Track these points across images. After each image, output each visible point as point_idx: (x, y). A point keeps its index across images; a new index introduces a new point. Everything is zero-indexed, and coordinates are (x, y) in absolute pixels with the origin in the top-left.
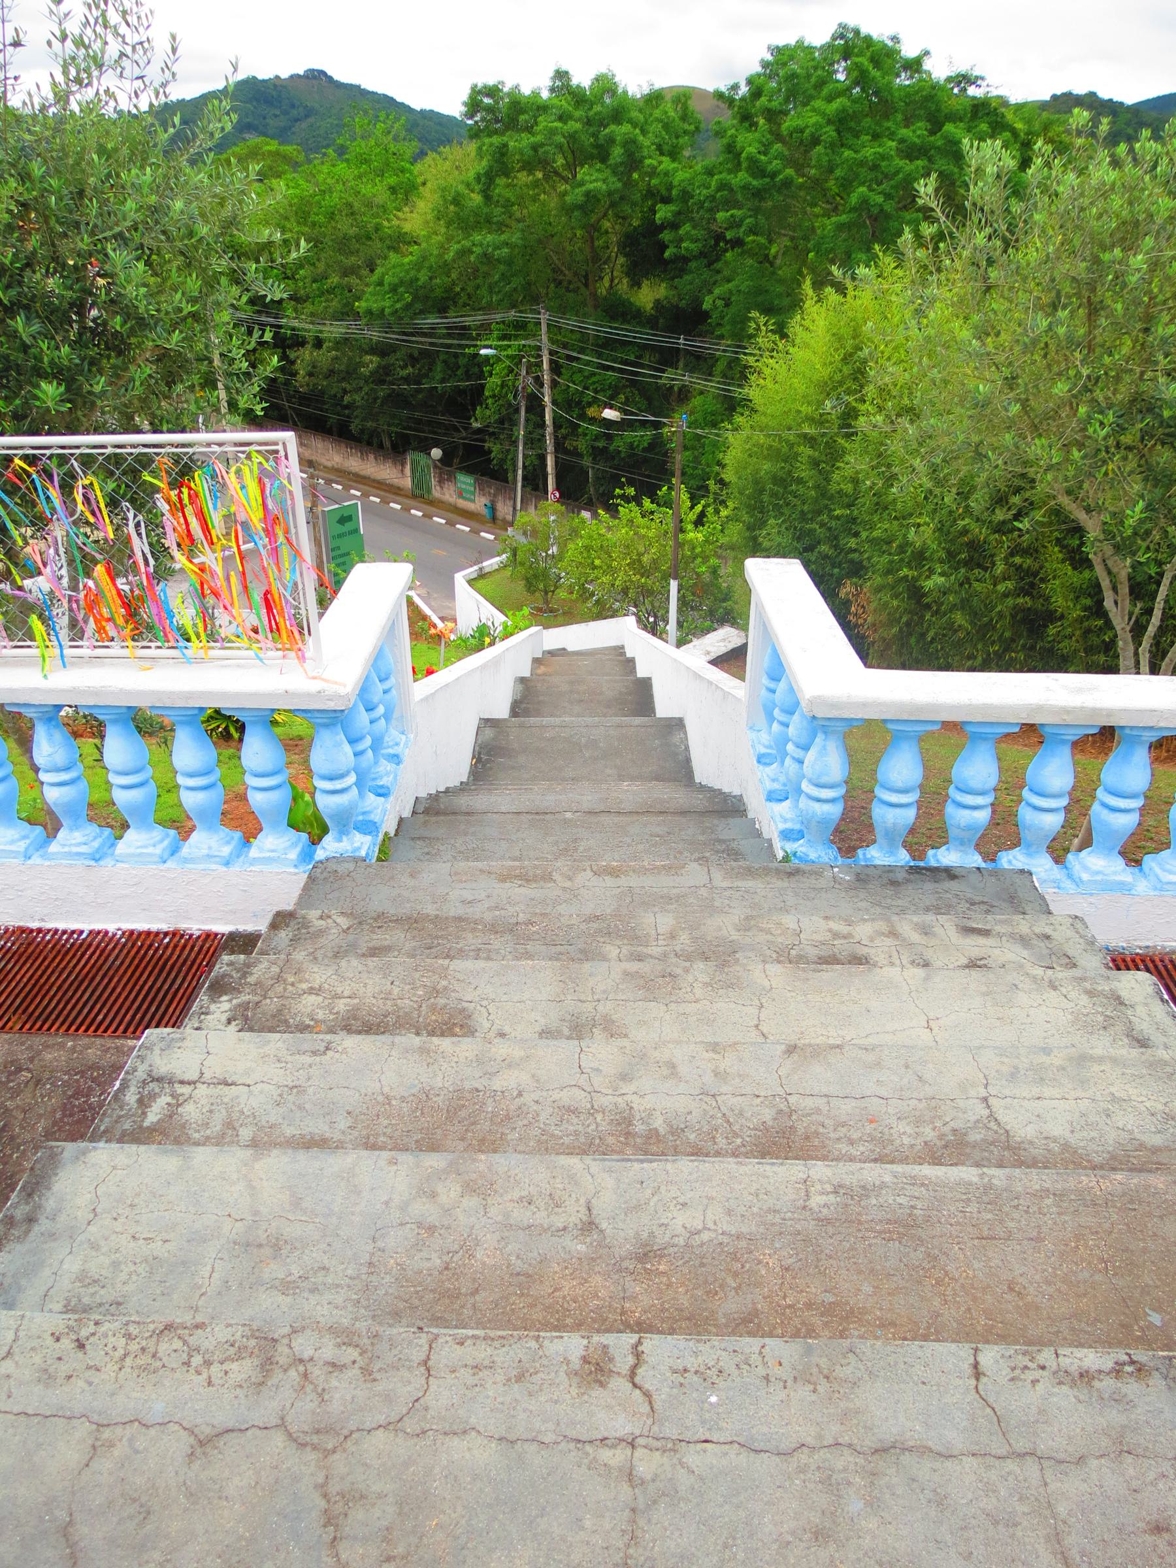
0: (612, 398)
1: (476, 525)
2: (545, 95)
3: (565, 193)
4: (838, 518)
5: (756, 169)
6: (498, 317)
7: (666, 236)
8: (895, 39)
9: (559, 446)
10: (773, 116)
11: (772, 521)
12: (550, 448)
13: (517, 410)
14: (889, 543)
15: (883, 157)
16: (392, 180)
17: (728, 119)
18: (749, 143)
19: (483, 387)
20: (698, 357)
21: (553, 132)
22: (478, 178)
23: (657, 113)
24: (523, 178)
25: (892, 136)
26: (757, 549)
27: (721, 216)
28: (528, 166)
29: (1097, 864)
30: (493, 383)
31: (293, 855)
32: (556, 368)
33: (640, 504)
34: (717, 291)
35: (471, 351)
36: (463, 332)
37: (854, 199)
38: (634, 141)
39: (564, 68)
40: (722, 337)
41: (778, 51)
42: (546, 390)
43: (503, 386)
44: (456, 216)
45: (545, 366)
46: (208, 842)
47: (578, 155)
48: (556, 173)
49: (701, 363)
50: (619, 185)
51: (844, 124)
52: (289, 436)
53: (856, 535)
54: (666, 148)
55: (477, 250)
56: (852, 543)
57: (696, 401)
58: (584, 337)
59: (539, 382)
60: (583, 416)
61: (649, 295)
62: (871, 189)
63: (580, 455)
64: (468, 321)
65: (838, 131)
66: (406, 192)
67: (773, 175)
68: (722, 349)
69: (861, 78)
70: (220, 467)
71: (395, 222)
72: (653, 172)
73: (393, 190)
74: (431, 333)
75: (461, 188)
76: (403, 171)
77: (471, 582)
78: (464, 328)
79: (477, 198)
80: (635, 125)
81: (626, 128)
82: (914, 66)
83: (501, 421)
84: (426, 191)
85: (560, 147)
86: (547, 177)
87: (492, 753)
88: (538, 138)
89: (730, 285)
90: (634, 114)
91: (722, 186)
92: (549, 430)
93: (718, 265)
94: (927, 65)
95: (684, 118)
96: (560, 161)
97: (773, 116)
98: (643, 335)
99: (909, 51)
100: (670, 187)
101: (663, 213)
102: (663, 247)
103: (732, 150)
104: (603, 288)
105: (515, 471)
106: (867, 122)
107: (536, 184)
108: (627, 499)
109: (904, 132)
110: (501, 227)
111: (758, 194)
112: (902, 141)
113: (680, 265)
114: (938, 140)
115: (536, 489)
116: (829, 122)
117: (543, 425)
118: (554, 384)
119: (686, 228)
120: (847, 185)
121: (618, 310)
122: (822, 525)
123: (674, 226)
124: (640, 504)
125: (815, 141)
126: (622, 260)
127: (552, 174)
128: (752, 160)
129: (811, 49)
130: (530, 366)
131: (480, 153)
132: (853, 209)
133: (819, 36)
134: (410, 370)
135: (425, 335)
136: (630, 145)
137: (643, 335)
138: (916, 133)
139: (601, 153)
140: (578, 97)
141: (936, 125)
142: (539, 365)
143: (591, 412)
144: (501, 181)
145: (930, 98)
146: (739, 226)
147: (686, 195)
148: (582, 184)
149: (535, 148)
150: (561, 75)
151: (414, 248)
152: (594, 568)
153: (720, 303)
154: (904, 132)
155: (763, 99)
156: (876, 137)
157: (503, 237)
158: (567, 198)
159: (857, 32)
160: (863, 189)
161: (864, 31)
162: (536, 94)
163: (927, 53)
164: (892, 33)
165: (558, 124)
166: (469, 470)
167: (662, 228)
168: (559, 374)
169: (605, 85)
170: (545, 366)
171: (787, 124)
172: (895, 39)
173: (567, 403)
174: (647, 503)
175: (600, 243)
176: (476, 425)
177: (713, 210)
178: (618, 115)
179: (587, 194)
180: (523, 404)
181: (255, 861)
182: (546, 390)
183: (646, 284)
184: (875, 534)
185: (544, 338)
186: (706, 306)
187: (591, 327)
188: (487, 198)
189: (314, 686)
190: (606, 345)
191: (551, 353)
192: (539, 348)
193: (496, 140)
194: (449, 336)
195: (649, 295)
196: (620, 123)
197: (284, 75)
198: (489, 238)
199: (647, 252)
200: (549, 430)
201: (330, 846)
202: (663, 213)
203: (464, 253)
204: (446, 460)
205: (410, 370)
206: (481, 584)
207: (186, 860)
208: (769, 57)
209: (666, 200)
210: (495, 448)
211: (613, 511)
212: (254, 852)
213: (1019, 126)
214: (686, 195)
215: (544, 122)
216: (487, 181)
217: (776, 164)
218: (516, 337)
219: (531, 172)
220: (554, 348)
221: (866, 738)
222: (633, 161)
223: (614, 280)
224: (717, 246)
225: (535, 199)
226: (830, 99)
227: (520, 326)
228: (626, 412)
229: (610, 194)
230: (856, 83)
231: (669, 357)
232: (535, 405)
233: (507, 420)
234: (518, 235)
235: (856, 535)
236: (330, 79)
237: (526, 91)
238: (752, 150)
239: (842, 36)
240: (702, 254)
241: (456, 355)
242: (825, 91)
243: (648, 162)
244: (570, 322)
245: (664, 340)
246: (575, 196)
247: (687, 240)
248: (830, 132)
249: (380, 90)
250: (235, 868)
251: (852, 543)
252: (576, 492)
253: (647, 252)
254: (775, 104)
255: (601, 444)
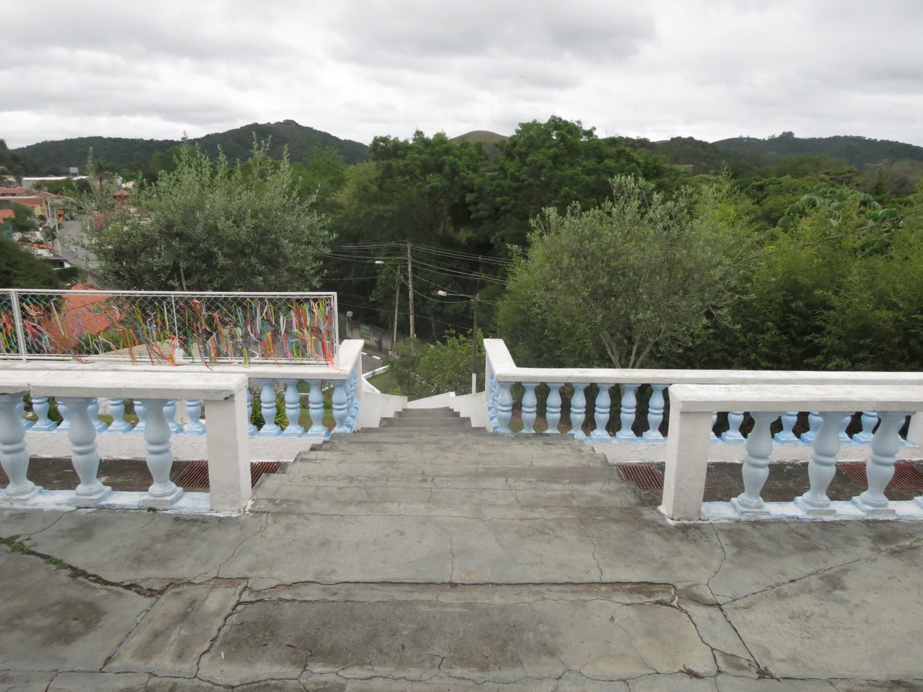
0: (445, 286)
1: (371, 352)
2: (411, 142)
3: (420, 187)
4: (551, 341)
5: (515, 178)
6: (385, 245)
7: (471, 208)
8: (579, 122)
9: (416, 310)
10: (523, 156)
11: (521, 343)
12: (412, 311)
13: (395, 292)
14: (574, 352)
15: (575, 174)
16: (332, 177)
17: (501, 156)
18: (512, 167)
19: (375, 280)
20: (490, 266)
21: (415, 159)
22: (376, 179)
23: (467, 151)
24: (399, 179)
25: (579, 165)
26: (487, 337)
27: (498, 199)
28: (402, 173)
29: (600, 433)
30: (382, 277)
31: (324, 433)
32: (415, 271)
33: (458, 338)
34: (497, 234)
35: (371, 262)
36: (366, 252)
37: (562, 192)
38: (455, 163)
39: (421, 130)
40: (500, 256)
41: (523, 125)
42: (410, 282)
43: (386, 279)
44: (363, 195)
45: (410, 270)
46: (293, 428)
47: (426, 169)
48: (416, 177)
49: (492, 269)
50: (448, 184)
51: (555, 158)
52: (335, 294)
53: (560, 349)
54: (471, 167)
55: (375, 213)
56: (558, 352)
57: (489, 288)
58: (430, 256)
59: (406, 278)
60: (429, 295)
61: (464, 235)
62: (571, 188)
63: (428, 315)
64: (369, 247)
65: (554, 163)
66: (338, 183)
67: (523, 181)
68: (500, 262)
69: (562, 138)
70: (312, 303)
71: (333, 198)
72: (464, 178)
73: (331, 182)
74: (349, 252)
75: (367, 183)
76: (337, 173)
77: (369, 380)
78: (367, 250)
79: (375, 188)
80: (455, 156)
81: (451, 158)
82: (589, 133)
83: (386, 298)
84: (349, 184)
85: (418, 166)
86: (411, 179)
87: (386, 422)
88: (408, 162)
89: (504, 232)
90: (456, 152)
91: (498, 186)
92: (411, 302)
93: (498, 222)
94: (595, 133)
95: (480, 153)
96: (418, 172)
97: (523, 156)
98: (461, 255)
99: (587, 127)
100: (473, 186)
101: (469, 197)
102: (470, 213)
103: (503, 169)
104: (440, 231)
105: (393, 323)
106: (567, 158)
107: (406, 182)
108: (451, 335)
109: (585, 163)
110: (387, 202)
111: (517, 190)
112: (584, 167)
113: (479, 222)
114: (601, 166)
115: (403, 333)
116: (549, 158)
117: (408, 299)
118: (414, 279)
119: (480, 205)
120: (561, 184)
121: (448, 242)
122: (545, 345)
123: (476, 204)
124: (458, 338)
125: (543, 166)
126: (449, 218)
127: (414, 178)
128: (512, 174)
129: (539, 125)
130: (402, 269)
131: (378, 168)
132: (563, 197)
133: (544, 119)
134: (337, 271)
135: (346, 253)
136: (453, 165)
137: (461, 255)
138: (591, 163)
139: (439, 168)
140: (427, 143)
141: (601, 158)
142: (406, 269)
143: (433, 293)
144: (388, 181)
145: (596, 148)
146: (507, 204)
147: (480, 190)
148: (429, 183)
149: (406, 166)
150: (419, 133)
151: (342, 211)
152: (434, 370)
153: (498, 240)
154: (585, 163)
155: (517, 147)
156: (572, 165)
157: (388, 208)
158: (422, 190)
159: (560, 119)
160: (566, 188)
161: (563, 119)
162: (406, 142)
163: (594, 128)
164: (577, 119)
165: (417, 156)
166: (367, 323)
167: (469, 204)
168: (417, 274)
169: (440, 138)
170: (410, 270)
171: (530, 158)
172: (579, 122)
173: (420, 287)
174: (462, 337)
175: (439, 209)
176: (372, 299)
177: (495, 196)
178: (447, 151)
179: (432, 187)
180: (398, 289)
181: (311, 435)
182: (410, 282)
183: (462, 230)
184: (568, 348)
185: (409, 256)
186: (492, 241)
187: (433, 251)
188: (380, 187)
189: (337, 372)
190: (441, 259)
191: (413, 263)
192: (406, 261)
193: (386, 162)
194: (359, 254)
195: (464, 235)
196: (448, 155)
197: (273, 122)
198: (381, 208)
199: (462, 214)
200: (411, 302)
201: (337, 430)
202: (469, 197)
203: (368, 214)
204: (354, 317)
205: (337, 271)
206: (374, 381)
207: (286, 435)
208: (520, 128)
209: (471, 191)
210: (382, 312)
211: (444, 342)
212: (309, 432)
213: (640, 161)
214: (480, 190)
215: (410, 155)
216: (381, 181)
217: (524, 176)
218: (395, 255)
219: (403, 176)
220: (415, 261)
221: (518, 389)
222: (455, 172)
223: (446, 227)
224: (496, 214)
225: (405, 188)
226: (549, 148)
227: (397, 251)
228: (448, 292)
229: (443, 187)
230: (561, 141)
231: (474, 266)
232: (404, 289)
233: (389, 296)
234: (397, 206)
235: (560, 349)
236: (297, 124)
237: (401, 140)
238: (512, 170)
239: (553, 121)
240: (490, 217)
241: (362, 264)
242: (546, 145)
243: (462, 174)
244: (423, 248)
245: (472, 258)
246: (427, 188)
247: (482, 210)
248: (549, 163)
249: (323, 131)
250: (302, 438)
251: (558, 352)
252: (425, 333)
253: (462, 214)
254: (522, 150)
255: (439, 309)
